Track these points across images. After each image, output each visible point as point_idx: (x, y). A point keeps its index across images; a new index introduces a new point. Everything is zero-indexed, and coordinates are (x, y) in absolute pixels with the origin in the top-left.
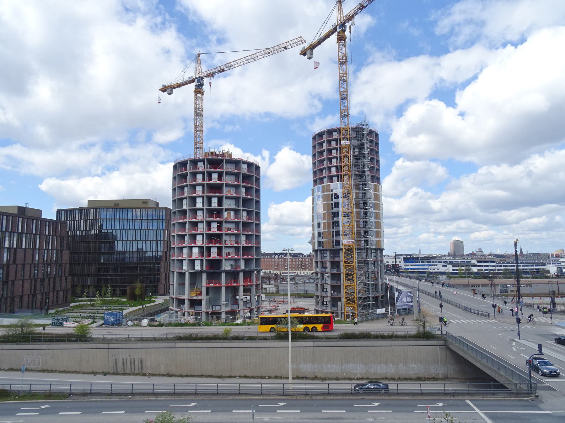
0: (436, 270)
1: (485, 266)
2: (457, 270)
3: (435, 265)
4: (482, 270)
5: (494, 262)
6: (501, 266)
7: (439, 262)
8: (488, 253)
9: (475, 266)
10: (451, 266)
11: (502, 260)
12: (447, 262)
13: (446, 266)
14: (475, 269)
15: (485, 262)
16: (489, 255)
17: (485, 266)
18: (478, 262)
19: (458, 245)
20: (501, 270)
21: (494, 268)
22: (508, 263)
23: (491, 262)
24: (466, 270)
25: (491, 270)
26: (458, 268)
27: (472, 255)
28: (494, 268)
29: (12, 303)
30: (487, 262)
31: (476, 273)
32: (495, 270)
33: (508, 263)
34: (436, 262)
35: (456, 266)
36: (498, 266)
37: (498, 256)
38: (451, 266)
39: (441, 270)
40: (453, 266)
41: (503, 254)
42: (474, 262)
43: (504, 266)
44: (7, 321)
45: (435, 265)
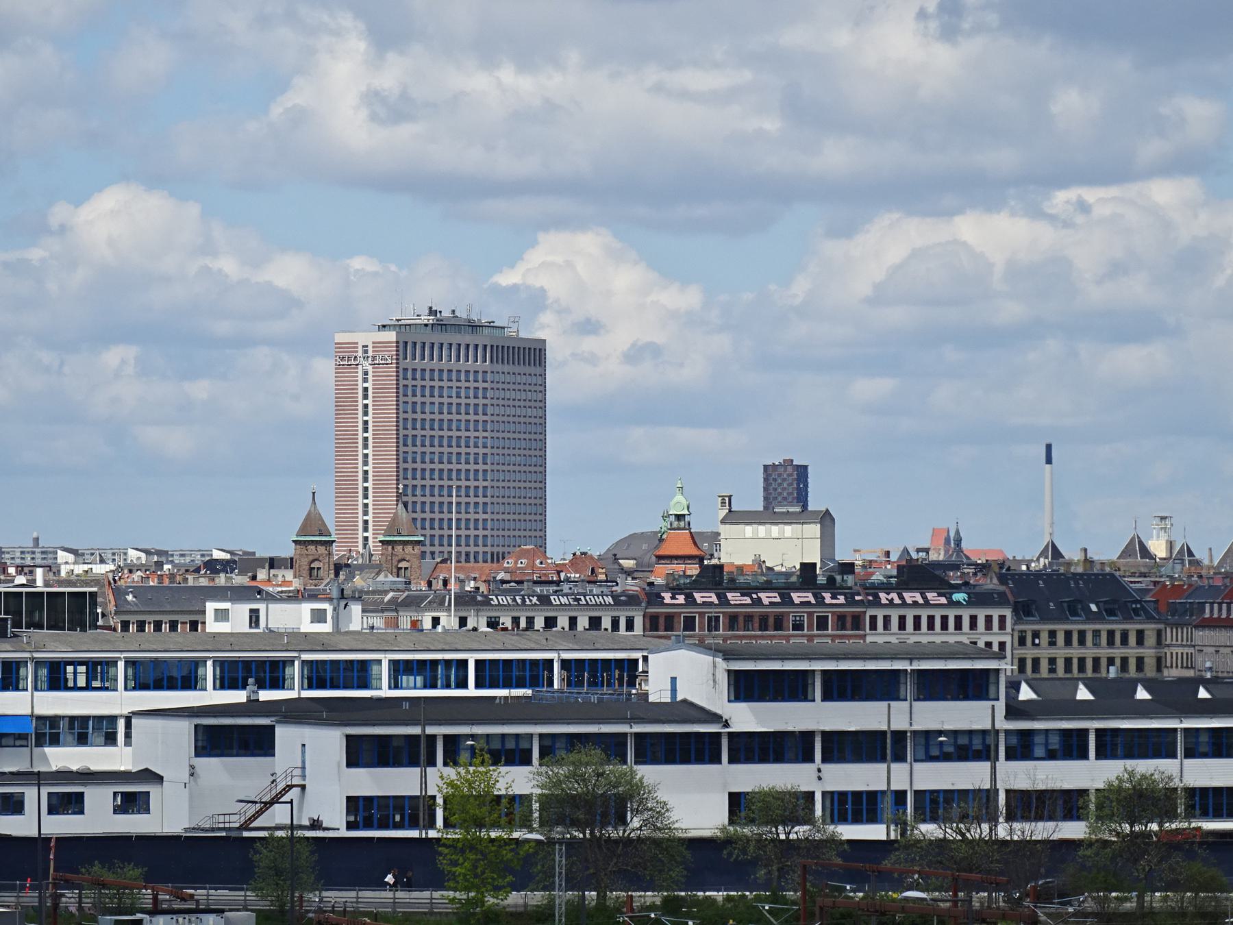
0: (99, 817)
1: (842, 747)
2: (415, 810)
3: (83, 730)
4: (796, 806)
5: (972, 686)
6: (1071, 747)
7: (150, 676)
8: (916, 537)
9: (698, 750)
10: (328, 742)
11: (1096, 643)
12: (273, 674)
13: (257, 742)
14: (693, 803)
15: (842, 687)
16: (916, 574)
17: (842, 747)
18: (746, 687)
19: (469, 395)
20: (1068, 803)
21: (968, 776)
22: (1175, 697)
23: (935, 686)
24: (559, 808)
25: (933, 804)
26: (438, 779)
27: (691, 592)
28: (968, 776)
29: (604, 815)
30: (881, 686)
31: (705, 857)
32: (979, 803)
33: (1175, 697)
34: (98, 674)
35: (410, 753)
36: (1022, 747)
37: (1049, 594)
38: (328, 742)
39: (169, 815)
40: (361, 753)
41: (1106, 550)
42: (683, 674)
43: (1111, 745)
44: (9, 897)
45: (83, 730)
